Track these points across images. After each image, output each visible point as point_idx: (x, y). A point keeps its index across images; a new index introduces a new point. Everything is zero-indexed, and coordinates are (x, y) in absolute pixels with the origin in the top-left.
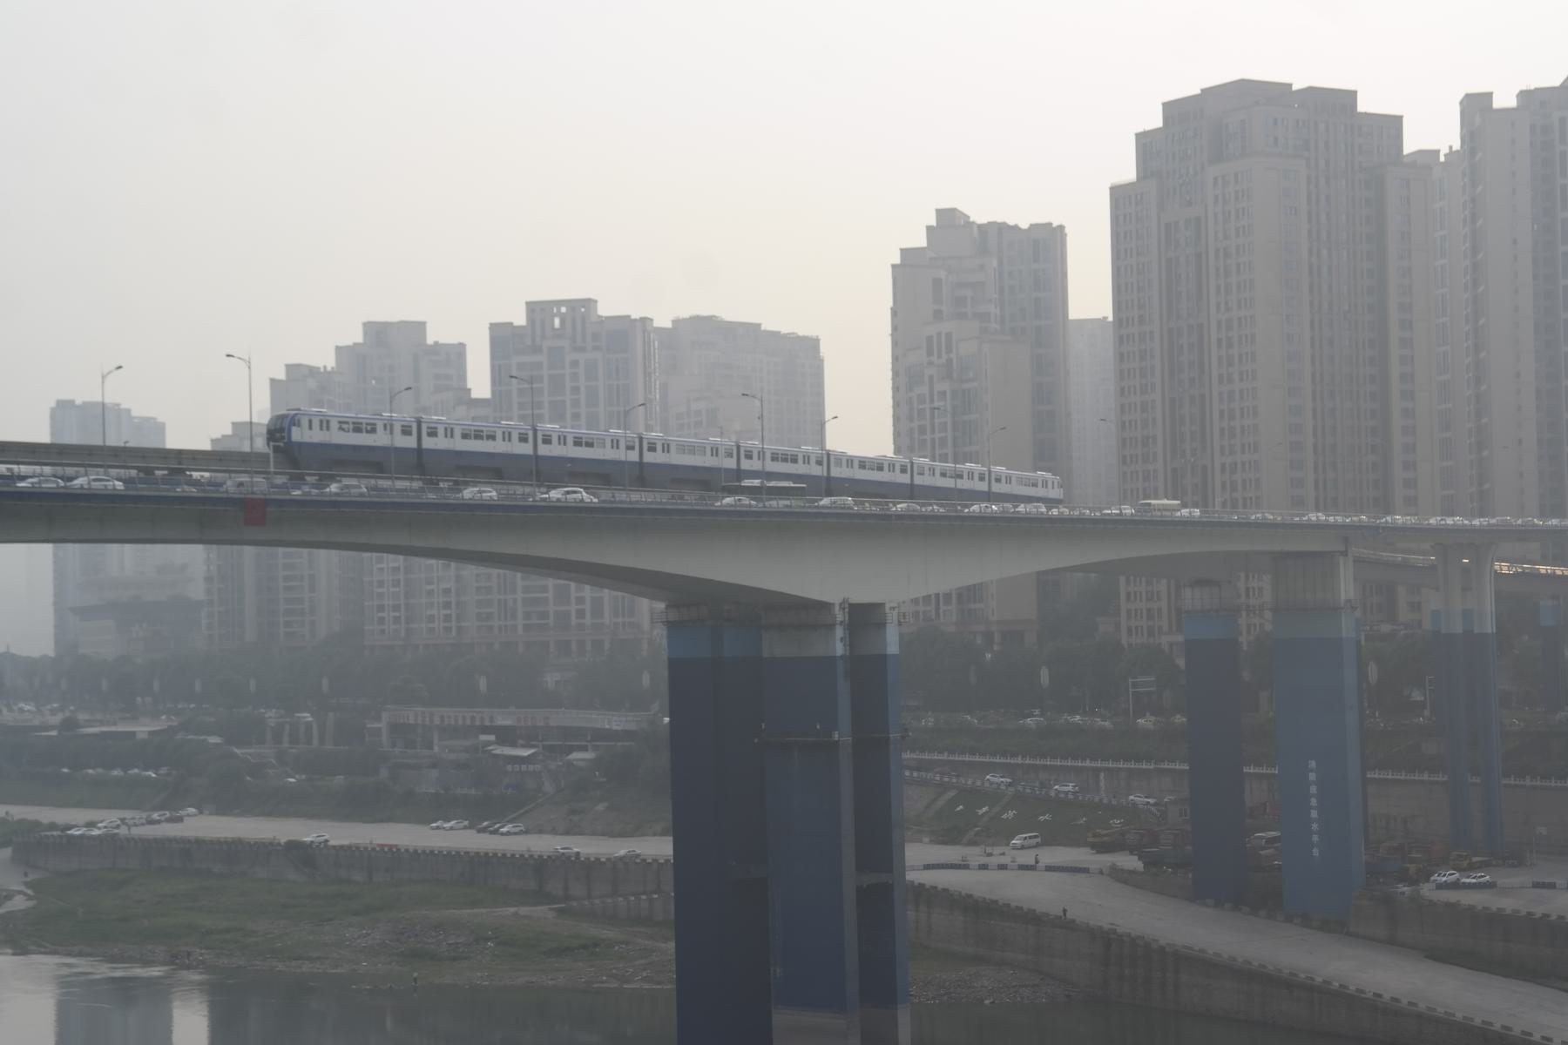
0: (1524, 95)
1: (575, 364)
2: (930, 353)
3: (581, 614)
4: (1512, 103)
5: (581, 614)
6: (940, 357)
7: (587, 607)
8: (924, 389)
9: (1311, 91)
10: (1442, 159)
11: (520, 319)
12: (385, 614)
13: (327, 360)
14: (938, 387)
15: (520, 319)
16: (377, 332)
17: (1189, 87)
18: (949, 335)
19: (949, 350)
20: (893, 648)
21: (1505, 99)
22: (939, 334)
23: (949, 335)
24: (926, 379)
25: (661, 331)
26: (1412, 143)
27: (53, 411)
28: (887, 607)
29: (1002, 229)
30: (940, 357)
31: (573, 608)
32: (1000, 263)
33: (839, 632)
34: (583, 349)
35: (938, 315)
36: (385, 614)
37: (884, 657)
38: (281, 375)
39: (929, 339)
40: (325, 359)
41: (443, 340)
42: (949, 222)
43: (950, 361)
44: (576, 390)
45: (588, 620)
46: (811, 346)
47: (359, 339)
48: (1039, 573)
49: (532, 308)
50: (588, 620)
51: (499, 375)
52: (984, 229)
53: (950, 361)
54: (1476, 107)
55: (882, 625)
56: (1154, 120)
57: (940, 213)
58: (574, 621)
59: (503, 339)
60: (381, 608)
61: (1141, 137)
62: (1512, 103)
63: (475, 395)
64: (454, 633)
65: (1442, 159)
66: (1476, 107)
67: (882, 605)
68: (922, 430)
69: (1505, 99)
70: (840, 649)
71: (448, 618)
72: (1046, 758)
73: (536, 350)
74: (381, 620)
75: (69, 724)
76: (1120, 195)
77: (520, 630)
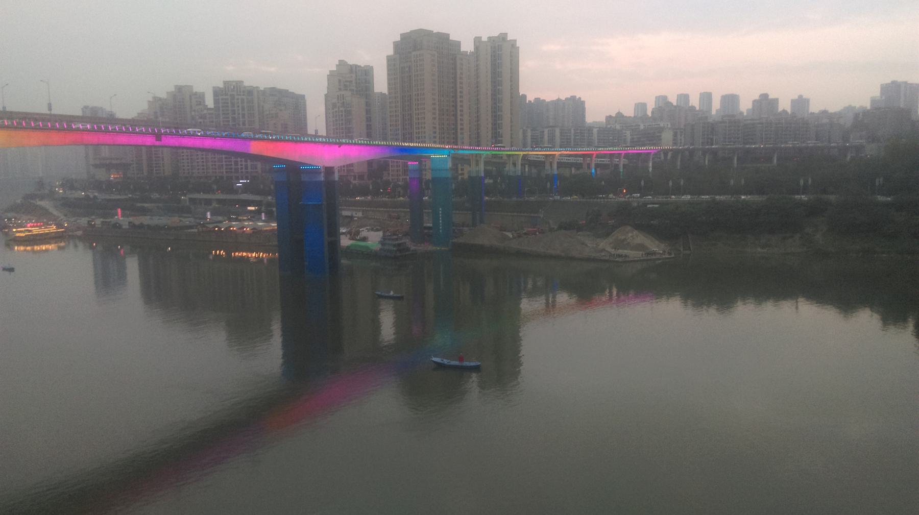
0: (489, 38)
1: (238, 99)
2: (338, 100)
4: (486, 40)
6: (341, 100)
7: (243, 166)
8: (337, 109)
9: (438, 33)
10: (468, 53)
12: (202, 167)
14: (341, 109)
17: (407, 30)
18: (343, 95)
19: (343, 99)
20: (337, 179)
21: (484, 39)
22: (340, 95)
23: (343, 95)
24: (337, 107)
25: (261, 91)
26: (463, 49)
27: (474, 39)
28: (335, 168)
29: (356, 66)
30: (341, 100)
32: (356, 76)
33: (322, 174)
34: (240, 95)
35: (340, 89)
36: (202, 167)
37: (334, 181)
38: (151, 99)
39: (338, 96)
40: (163, 95)
41: (198, 91)
42: (342, 63)
43: (344, 102)
44: (238, 106)
45: (244, 170)
46: (303, 97)
47: (173, 90)
48: (367, 161)
49: (225, 83)
50: (244, 170)
51: (216, 101)
52: (351, 66)
53: (344, 102)
54: (477, 40)
55: (333, 173)
56: (398, 39)
57: (340, 61)
58: (240, 171)
59: (217, 93)
61: (449, 35)
62: (486, 40)
63: (209, 107)
64: (205, 173)
65: (468, 53)
66: (477, 40)
67: (334, 167)
68: (336, 120)
69: (484, 39)
70: (323, 179)
71: (188, 163)
72: (200, 193)
73: (226, 95)
74: (184, 170)
76: (389, 59)
77: (225, 173)
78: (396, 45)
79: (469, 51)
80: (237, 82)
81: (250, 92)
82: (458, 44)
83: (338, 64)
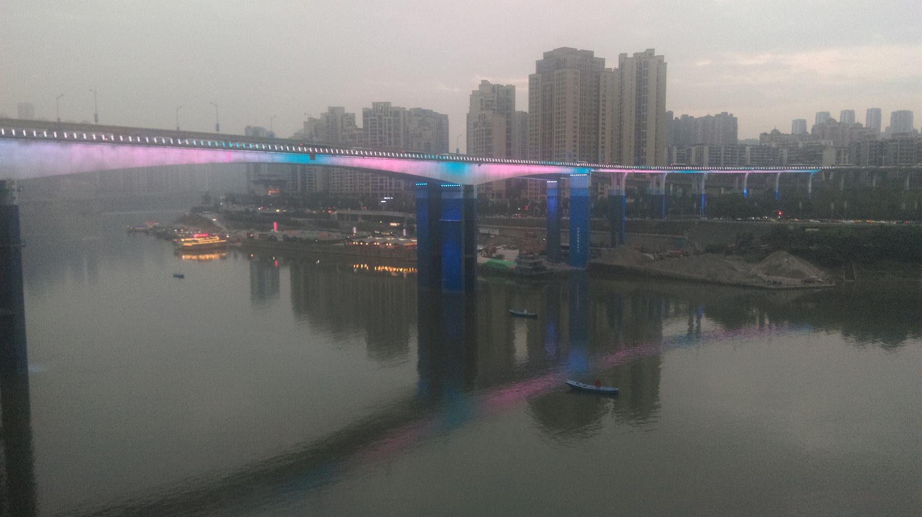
1: (385, 120)
2: (479, 119)
3: (386, 186)
5: (386, 186)
6: (482, 120)
10: (613, 71)
11: (371, 107)
13: (318, 117)
15: (371, 107)
16: (333, 110)
18: (485, 114)
21: (630, 55)
30: (482, 120)
31: (384, 185)
33: (462, 192)
34: (387, 116)
44: (385, 127)
49: (374, 104)
51: (365, 122)
54: (623, 58)
55: (473, 191)
58: (384, 188)
59: (366, 114)
60: (334, 183)
66: (623, 58)
69: (630, 55)
71: (351, 186)
73: (375, 116)
74: (334, 187)
75: (598, 179)
76: (531, 78)
77: (370, 190)
78: (539, 65)
79: (613, 68)
80: (385, 103)
81: (397, 113)
82: (602, 61)
83: (481, 84)
